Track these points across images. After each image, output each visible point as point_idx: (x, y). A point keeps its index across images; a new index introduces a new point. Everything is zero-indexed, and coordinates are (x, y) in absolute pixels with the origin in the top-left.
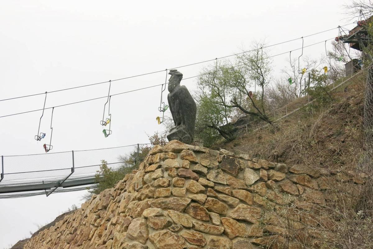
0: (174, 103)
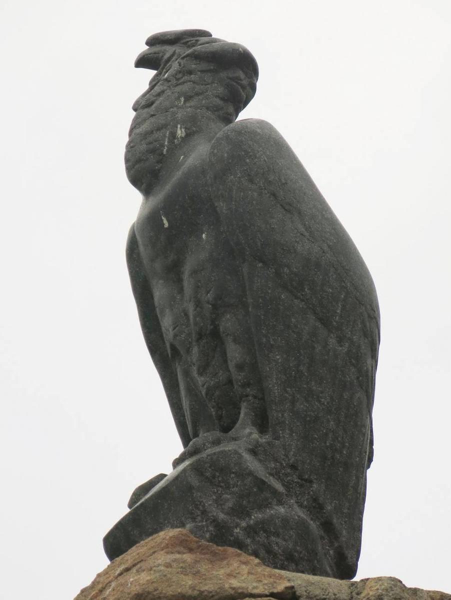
0: (173, 272)
